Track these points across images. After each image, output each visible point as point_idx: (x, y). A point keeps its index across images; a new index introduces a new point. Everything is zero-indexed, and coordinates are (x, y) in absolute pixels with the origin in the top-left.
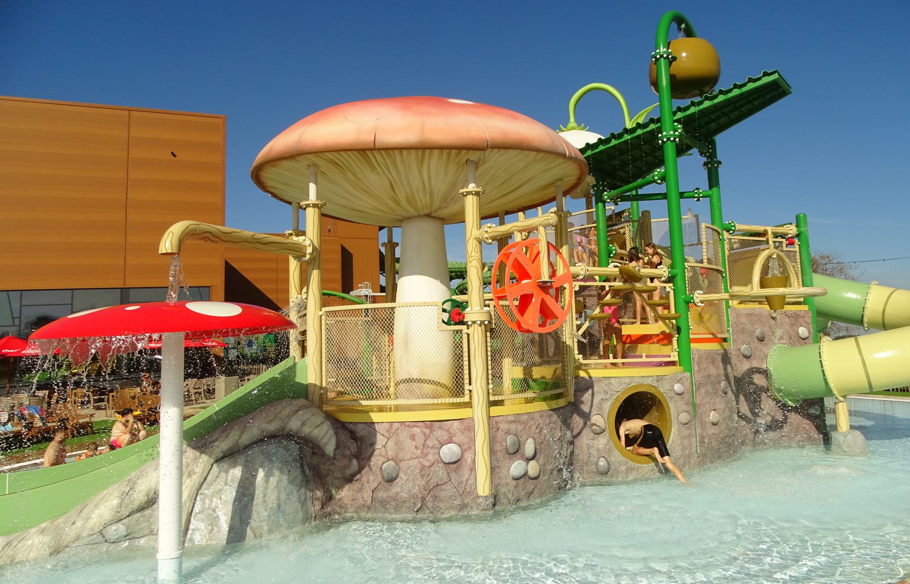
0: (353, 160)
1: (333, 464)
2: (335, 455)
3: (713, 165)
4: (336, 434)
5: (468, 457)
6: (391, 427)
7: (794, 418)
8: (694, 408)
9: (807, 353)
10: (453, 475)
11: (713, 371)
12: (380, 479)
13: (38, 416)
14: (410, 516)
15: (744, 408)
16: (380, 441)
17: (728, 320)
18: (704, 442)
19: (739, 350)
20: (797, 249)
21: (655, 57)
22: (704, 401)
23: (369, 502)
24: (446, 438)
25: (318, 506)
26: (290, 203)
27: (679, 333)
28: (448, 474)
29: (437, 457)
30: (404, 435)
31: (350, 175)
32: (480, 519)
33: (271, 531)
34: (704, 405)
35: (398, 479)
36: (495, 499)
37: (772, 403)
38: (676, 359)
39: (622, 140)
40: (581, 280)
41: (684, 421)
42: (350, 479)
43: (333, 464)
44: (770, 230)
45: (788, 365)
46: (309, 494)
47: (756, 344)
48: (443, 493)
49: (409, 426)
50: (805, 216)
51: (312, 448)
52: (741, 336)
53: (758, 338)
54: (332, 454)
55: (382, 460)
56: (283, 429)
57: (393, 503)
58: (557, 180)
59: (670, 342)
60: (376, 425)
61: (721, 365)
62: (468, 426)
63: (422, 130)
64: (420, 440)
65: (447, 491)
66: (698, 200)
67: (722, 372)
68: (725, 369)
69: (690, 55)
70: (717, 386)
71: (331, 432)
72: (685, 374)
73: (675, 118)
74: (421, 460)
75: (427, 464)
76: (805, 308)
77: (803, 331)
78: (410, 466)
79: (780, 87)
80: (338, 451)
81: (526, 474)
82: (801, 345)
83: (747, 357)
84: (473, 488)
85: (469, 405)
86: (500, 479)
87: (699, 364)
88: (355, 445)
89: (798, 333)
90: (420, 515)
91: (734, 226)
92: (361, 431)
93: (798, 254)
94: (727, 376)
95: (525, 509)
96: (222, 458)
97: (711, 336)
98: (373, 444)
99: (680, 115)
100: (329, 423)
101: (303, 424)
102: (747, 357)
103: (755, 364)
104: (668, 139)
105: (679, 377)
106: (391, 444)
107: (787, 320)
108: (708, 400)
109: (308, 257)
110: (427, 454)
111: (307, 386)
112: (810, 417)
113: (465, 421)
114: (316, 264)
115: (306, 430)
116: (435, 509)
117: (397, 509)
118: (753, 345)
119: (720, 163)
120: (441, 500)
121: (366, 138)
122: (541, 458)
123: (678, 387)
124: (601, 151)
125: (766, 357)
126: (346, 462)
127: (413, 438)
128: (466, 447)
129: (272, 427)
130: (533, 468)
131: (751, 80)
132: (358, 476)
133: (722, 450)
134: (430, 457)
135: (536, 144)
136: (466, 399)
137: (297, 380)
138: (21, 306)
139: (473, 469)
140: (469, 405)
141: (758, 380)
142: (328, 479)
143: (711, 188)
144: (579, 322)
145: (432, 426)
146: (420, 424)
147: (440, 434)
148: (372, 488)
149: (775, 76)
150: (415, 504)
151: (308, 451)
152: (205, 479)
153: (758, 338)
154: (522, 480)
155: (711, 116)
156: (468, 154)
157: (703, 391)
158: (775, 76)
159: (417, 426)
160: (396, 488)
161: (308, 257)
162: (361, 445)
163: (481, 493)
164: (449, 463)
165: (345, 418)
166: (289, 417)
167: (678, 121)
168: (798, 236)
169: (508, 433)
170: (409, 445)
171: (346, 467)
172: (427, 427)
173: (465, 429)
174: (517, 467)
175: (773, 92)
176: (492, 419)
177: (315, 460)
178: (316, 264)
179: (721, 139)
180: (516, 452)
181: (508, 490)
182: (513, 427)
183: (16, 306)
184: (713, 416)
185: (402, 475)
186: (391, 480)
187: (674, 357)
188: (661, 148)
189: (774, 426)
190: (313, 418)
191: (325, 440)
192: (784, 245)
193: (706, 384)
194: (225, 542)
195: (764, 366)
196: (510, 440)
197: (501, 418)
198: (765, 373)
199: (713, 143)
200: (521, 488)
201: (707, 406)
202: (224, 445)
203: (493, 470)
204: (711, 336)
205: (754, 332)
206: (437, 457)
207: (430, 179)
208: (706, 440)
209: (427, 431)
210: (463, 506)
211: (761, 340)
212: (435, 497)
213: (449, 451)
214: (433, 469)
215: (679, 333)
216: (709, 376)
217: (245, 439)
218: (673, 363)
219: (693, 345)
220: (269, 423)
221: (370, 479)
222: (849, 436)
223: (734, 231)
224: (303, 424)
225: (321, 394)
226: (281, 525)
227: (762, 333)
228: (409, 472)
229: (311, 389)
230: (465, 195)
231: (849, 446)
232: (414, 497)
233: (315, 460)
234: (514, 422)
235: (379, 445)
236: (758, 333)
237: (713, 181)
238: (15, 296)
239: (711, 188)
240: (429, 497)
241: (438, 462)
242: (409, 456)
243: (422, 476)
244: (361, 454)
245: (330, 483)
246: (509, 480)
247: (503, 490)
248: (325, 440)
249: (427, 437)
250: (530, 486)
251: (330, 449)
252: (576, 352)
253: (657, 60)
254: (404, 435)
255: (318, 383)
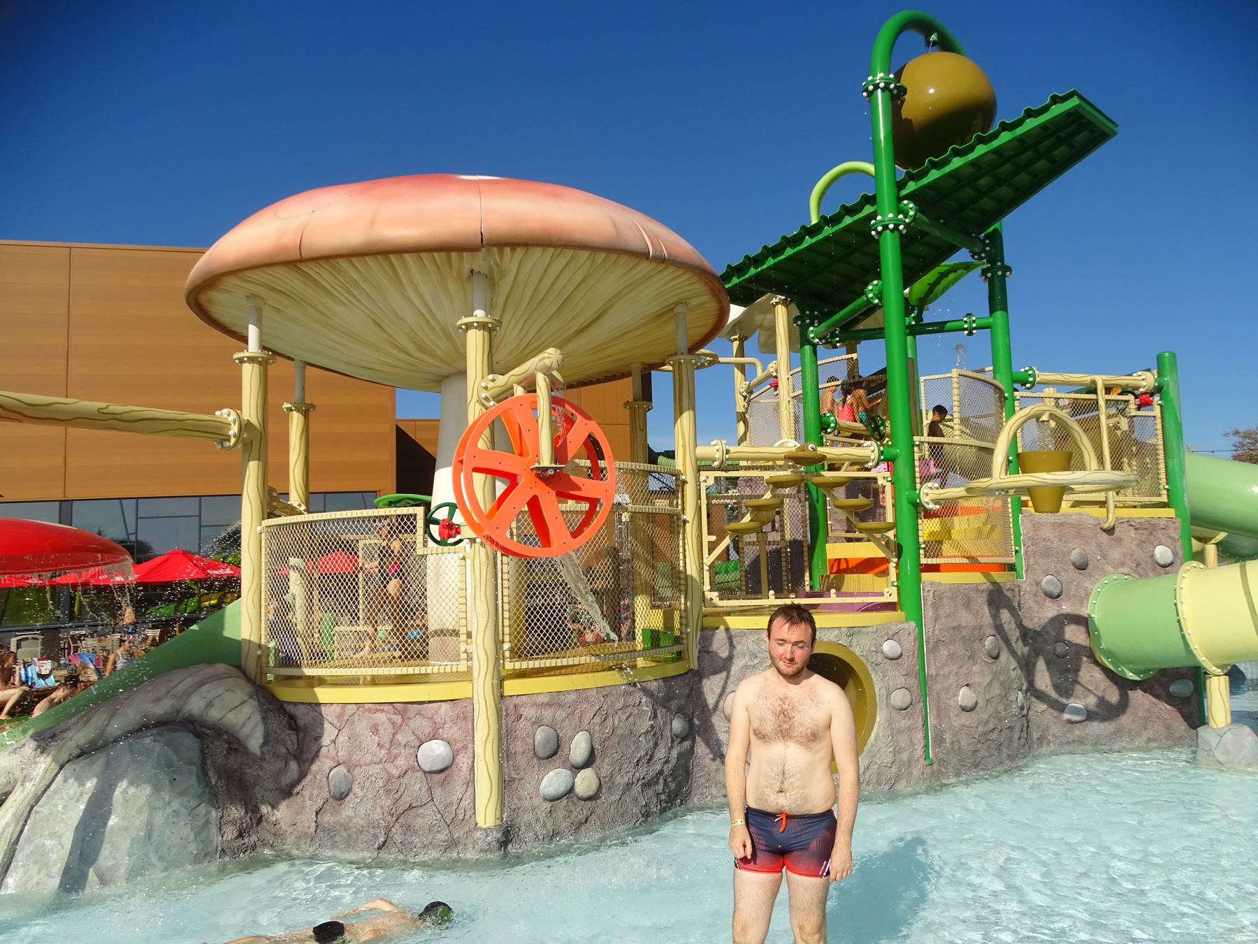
0: (287, 278)
1: (261, 767)
2: (263, 753)
3: (994, 273)
4: (264, 719)
5: (463, 761)
6: (342, 713)
7: (1137, 696)
8: (923, 684)
9: (1155, 587)
10: (438, 793)
11: (965, 619)
12: (326, 795)
13: (92, 666)
14: (367, 855)
15: (1043, 680)
16: (329, 733)
17: (1017, 534)
18: (943, 740)
19: (1038, 584)
20: (1157, 411)
21: (867, 90)
22: (946, 670)
23: (313, 829)
24: (428, 730)
25: (230, 832)
26: (292, 359)
27: (899, 556)
28: (430, 789)
29: (411, 761)
30: (362, 726)
31: (310, 310)
32: (477, 865)
33: (133, 874)
34: (947, 676)
35: (351, 795)
36: (507, 835)
37: (1098, 674)
38: (894, 599)
39: (821, 237)
40: (719, 469)
41: (899, 704)
42: (287, 792)
43: (261, 767)
44: (1100, 380)
45: (1122, 613)
46: (214, 814)
47: (1073, 573)
48: (420, 821)
49: (370, 711)
50: (1173, 356)
51: (229, 743)
52: (1041, 561)
53: (1074, 564)
54: (258, 752)
55: (329, 763)
56: (178, 712)
57: (345, 834)
58: (677, 303)
59: (885, 573)
60: (323, 708)
61: (986, 609)
62: (463, 710)
63: (372, 223)
64: (386, 733)
65: (426, 817)
66: (970, 334)
67: (987, 619)
68: (995, 616)
69: (936, 82)
70: (976, 645)
71: (257, 717)
72: (905, 626)
73: (903, 193)
74: (387, 765)
75: (395, 772)
76: (1170, 512)
77: (1162, 553)
78: (370, 774)
79: (1082, 117)
80: (265, 749)
81: (571, 790)
82: (1158, 575)
83: (1054, 597)
84: (469, 813)
85: (467, 676)
86: (520, 799)
87: (936, 607)
88: (294, 738)
89: (1153, 556)
90: (384, 855)
91: (1033, 375)
92: (303, 716)
93: (1159, 421)
94: (999, 628)
95: (566, 851)
96: (79, 756)
97: (965, 561)
98: (318, 738)
99: (912, 186)
100: (255, 703)
101: (210, 704)
102: (1054, 597)
103: (1066, 608)
104: (885, 227)
105: (894, 629)
106: (343, 738)
107: (1132, 533)
108: (954, 668)
109: (233, 440)
110: (396, 757)
111: (237, 645)
112: (1171, 699)
113: (459, 704)
114: (255, 452)
115: (215, 714)
116: (405, 847)
117: (350, 844)
118: (1064, 576)
119: (1009, 269)
120: (415, 832)
121: (290, 239)
122: (605, 766)
123: (889, 647)
124: (790, 258)
125: (1088, 595)
126: (280, 764)
127: (375, 729)
128: (459, 745)
129: (161, 709)
130: (585, 782)
131: (1030, 114)
132: (299, 788)
133: (983, 753)
134: (401, 762)
135: (579, 235)
136: (463, 667)
137: (227, 633)
138: (137, 518)
139: (470, 782)
140: (467, 676)
141: (1074, 634)
142: (257, 789)
143: (992, 311)
144: (713, 538)
145: (405, 710)
146: (386, 707)
147: (420, 724)
148: (315, 808)
149: (1075, 101)
150: (376, 836)
151: (219, 747)
152: (48, 787)
153: (1074, 564)
154: (564, 801)
155: (971, 186)
156: (474, 259)
157: (943, 653)
158: (1075, 101)
159: (382, 711)
160: (347, 811)
161: (233, 440)
162: (305, 736)
163: (481, 824)
164: (432, 772)
165: (286, 694)
166: (188, 693)
167: (909, 197)
168: (1158, 390)
169: (538, 723)
170: (370, 741)
171: (280, 773)
172: (397, 712)
173: (458, 717)
174: (553, 780)
175: (1076, 136)
176: (507, 701)
177: (234, 762)
178: (255, 452)
179: (1011, 226)
180: (555, 752)
181: (532, 818)
182: (548, 713)
183: (130, 518)
184: (965, 696)
185: (356, 789)
186: (341, 797)
187: (891, 596)
188: (875, 243)
189: (1107, 712)
190: (229, 696)
191: (246, 730)
192: (1132, 406)
193: (953, 641)
194: (55, 882)
195: (1084, 612)
196: (540, 735)
197: (524, 698)
198: (1083, 621)
199: (996, 238)
200: (561, 813)
201: (952, 679)
202: (80, 736)
203: (506, 784)
204: (965, 561)
205: (1069, 553)
206: (411, 761)
207: (427, 306)
208: (948, 736)
209: (398, 719)
210: (452, 844)
211: (1081, 567)
212: (408, 828)
213: (434, 752)
214: (405, 780)
215: (899, 556)
216: (957, 628)
217: (115, 727)
218: (891, 606)
219: (926, 576)
220: (157, 700)
221: (311, 793)
222: (1229, 737)
223: (1033, 384)
224: (210, 704)
225: (259, 657)
226: (153, 865)
227: (1084, 555)
228: (367, 785)
229: (245, 648)
230: (469, 326)
231: (1227, 752)
232: (375, 826)
233: (234, 762)
234: (549, 705)
235: (326, 741)
236: (1075, 555)
237: (997, 301)
238: (129, 506)
239: (992, 311)
240: (397, 826)
241: (413, 769)
242: (368, 758)
243: (388, 792)
244: (302, 752)
245: (259, 796)
246: (537, 801)
247: (526, 818)
248: (246, 730)
249: (397, 729)
250: (579, 812)
251: (255, 743)
252: (707, 587)
253: (870, 94)
254: (362, 726)
255: (254, 639)
